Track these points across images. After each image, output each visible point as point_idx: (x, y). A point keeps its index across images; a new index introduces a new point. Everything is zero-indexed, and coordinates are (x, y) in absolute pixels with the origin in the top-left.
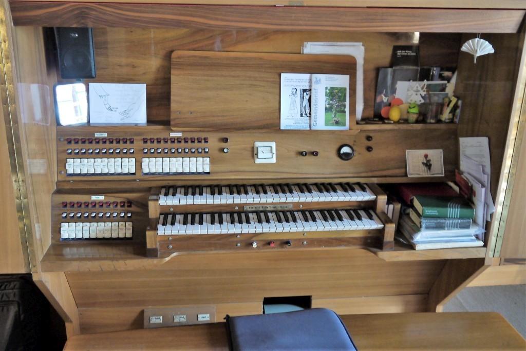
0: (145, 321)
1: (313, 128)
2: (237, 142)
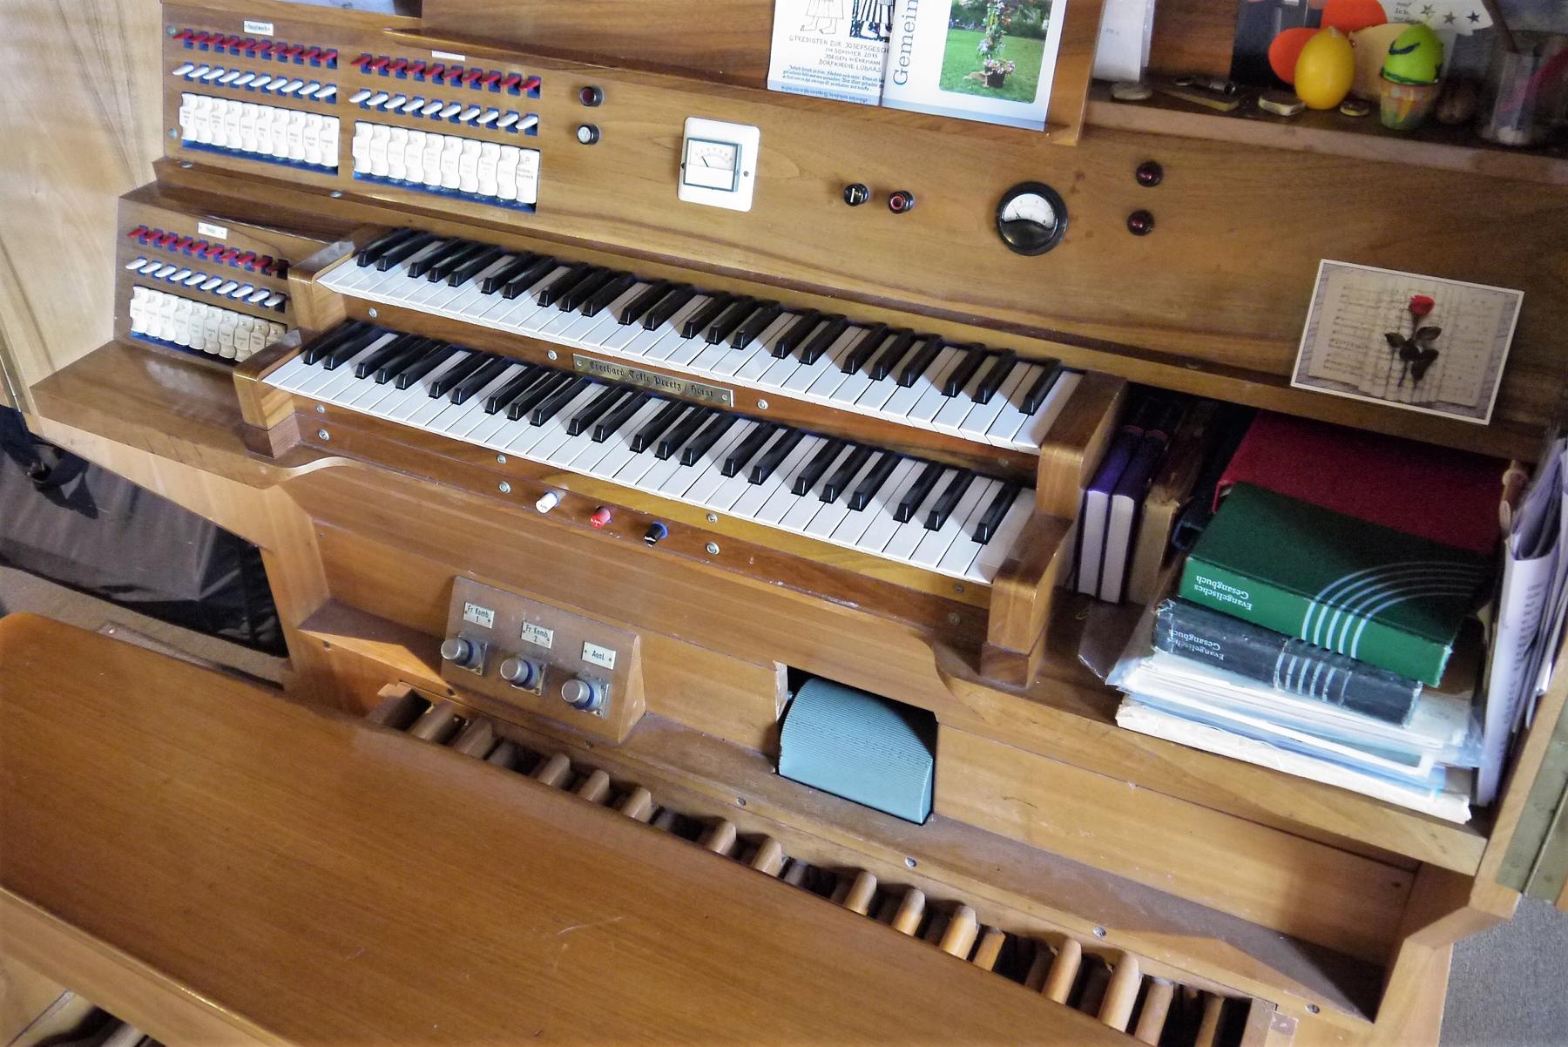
2: (631, 105)
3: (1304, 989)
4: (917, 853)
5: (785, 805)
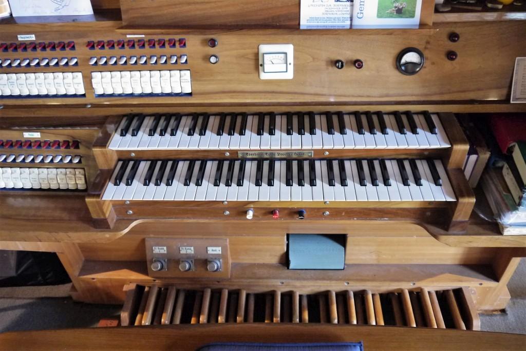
0: (147, 251)
1: (357, 23)
2: (230, 45)
3: (476, 279)
4: (348, 280)
5: (298, 279)
